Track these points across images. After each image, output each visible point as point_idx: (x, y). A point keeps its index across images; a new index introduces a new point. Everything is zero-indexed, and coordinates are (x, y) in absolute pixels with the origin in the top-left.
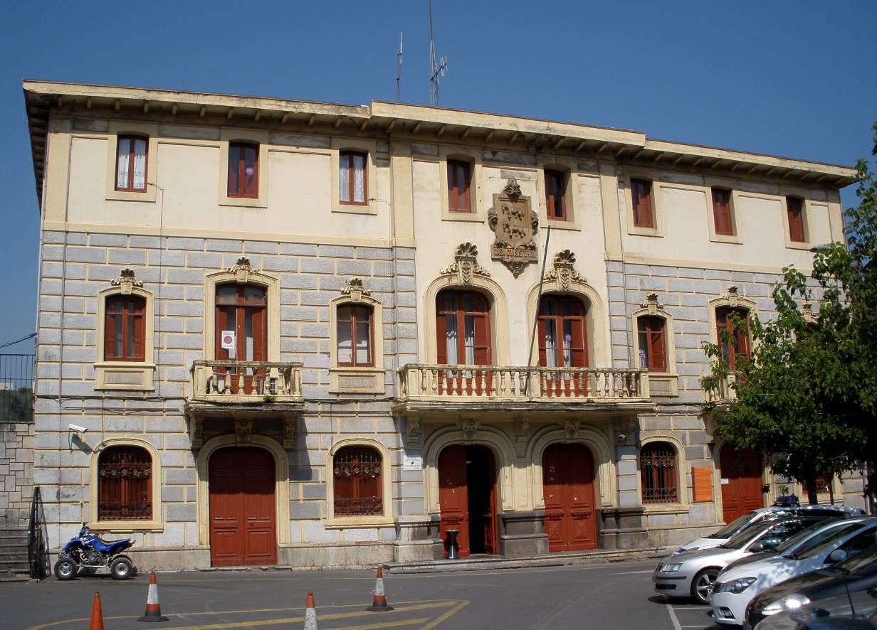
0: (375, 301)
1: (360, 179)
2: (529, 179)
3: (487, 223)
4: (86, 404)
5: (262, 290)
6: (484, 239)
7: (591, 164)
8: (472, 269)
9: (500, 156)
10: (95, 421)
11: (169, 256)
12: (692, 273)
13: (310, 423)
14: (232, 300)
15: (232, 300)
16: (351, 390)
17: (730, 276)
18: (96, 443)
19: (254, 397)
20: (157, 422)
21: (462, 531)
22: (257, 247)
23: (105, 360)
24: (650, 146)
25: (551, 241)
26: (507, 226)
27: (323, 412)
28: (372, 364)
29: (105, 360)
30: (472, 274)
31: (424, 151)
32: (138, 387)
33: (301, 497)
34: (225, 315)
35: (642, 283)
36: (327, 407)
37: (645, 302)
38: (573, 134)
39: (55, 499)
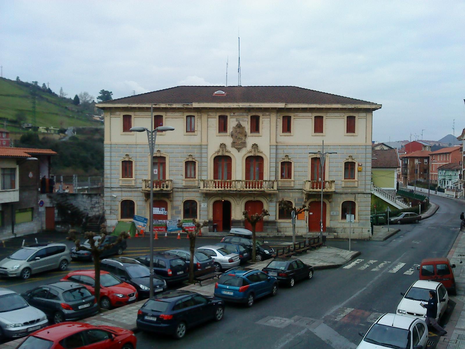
0: (196, 160)
1: (192, 122)
2: (245, 121)
3: (230, 136)
4: (118, 189)
5: (164, 158)
6: (228, 140)
7: (267, 114)
8: (224, 150)
9: (236, 114)
10: (119, 194)
11: (139, 150)
12: (303, 147)
13: (154, 262)
14: (156, 161)
15: (156, 161)
16: (189, 185)
17: (317, 147)
18: (120, 199)
19: (158, 189)
20: (136, 194)
21: (221, 224)
22: (163, 146)
23: (122, 178)
24: (289, 106)
25: (251, 140)
26: (237, 137)
27: (180, 191)
28: (195, 178)
29: (122, 178)
30: (224, 152)
31: (212, 115)
32: (130, 185)
33: (174, 213)
34: (154, 164)
35: (283, 151)
36: (182, 190)
37: (348, 158)
38: (258, 106)
39: (109, 213)
